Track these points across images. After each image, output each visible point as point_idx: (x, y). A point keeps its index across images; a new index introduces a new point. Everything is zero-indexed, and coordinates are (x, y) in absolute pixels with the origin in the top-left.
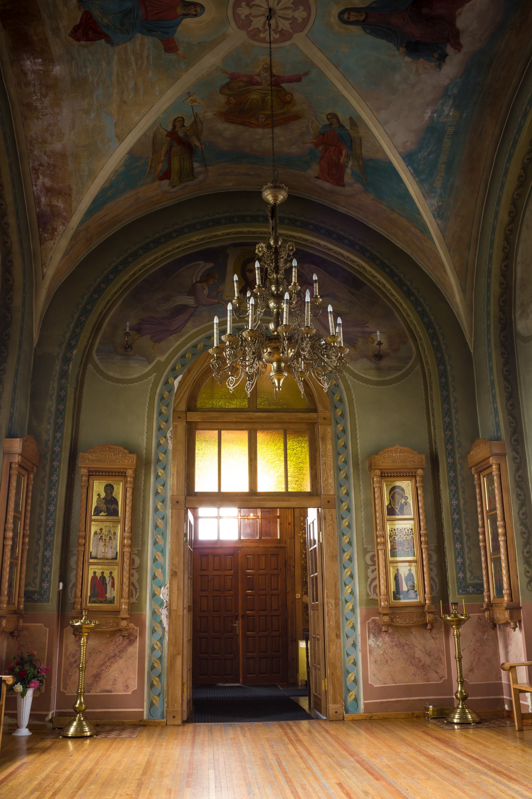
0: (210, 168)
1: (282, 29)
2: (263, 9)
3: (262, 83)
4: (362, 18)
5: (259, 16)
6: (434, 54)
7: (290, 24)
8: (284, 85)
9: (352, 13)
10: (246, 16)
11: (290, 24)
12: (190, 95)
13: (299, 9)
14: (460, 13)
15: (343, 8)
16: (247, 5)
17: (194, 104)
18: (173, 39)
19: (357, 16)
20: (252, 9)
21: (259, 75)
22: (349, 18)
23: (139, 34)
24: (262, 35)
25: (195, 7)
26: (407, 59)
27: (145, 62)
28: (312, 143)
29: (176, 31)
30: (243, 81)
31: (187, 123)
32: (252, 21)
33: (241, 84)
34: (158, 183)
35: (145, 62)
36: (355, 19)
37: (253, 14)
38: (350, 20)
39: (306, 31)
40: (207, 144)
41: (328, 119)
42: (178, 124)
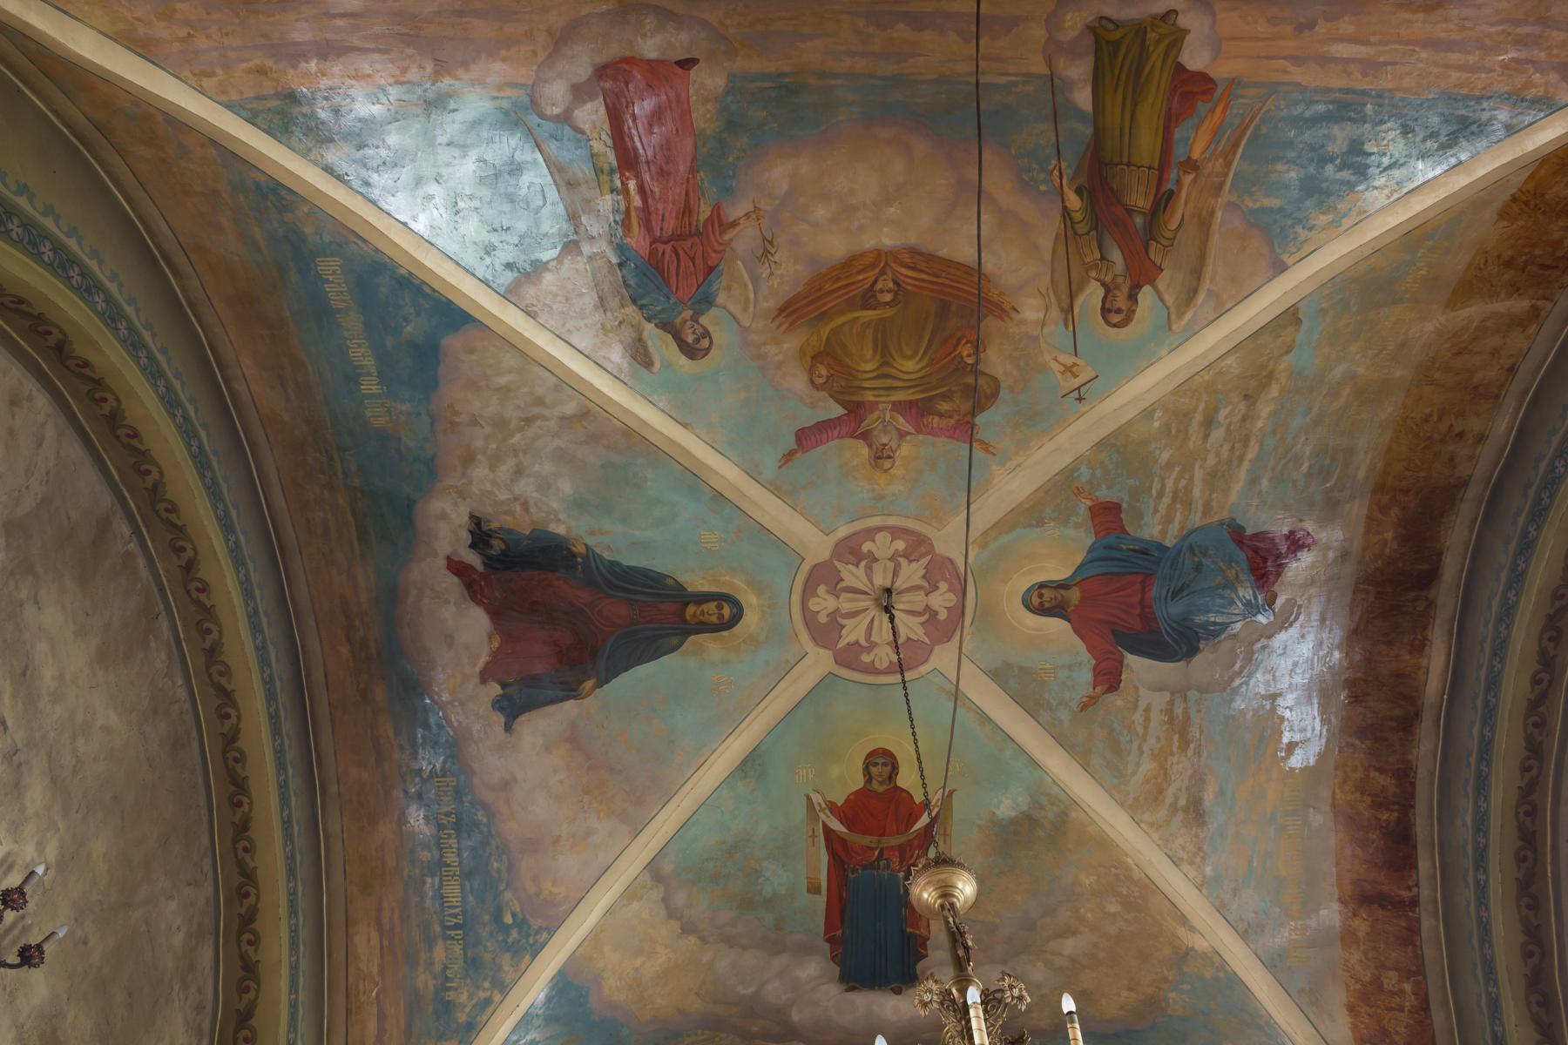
0: (1040, 68)
1: (857, 565)
2: (901, 606)
3: (892, 410)
4: (691, 609)
5: (908, 590)
6: (503, 547)
7: (842, 580)
8: (838, 411)
9: (714, 619)
10: (937, 588)
11: (842, 580)
12: (1076, 394)
13: (828, 616)
14: (490, 637)
15: (736, 629)
16: (936, 613)
17: (1069, 360)
18: (1096, 534)
19: (703, 613)
20: (925, 604)
21: (902, 435)
22: (720, 607)
23: (1169, 545)
24: (900, 545)
25: (1041, 604)
26: (561, 530)
27: (1169, 485)
28: (734, 224)
29: (1089, 552)
30: (941, 415)
31: (1093, 294)
32: (924, 577)
33: (945, 407)
34: (1221, 71)
35: (1169, 485)
36: (705, 607)
37: (922, 593)
38: (716, 603)
39: (806, 568)
40: (1043, 188)
41: (706, 334)
42: (1121, 302)
